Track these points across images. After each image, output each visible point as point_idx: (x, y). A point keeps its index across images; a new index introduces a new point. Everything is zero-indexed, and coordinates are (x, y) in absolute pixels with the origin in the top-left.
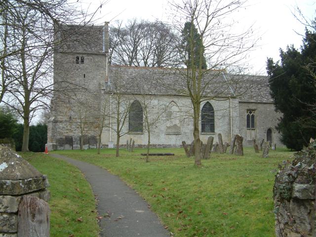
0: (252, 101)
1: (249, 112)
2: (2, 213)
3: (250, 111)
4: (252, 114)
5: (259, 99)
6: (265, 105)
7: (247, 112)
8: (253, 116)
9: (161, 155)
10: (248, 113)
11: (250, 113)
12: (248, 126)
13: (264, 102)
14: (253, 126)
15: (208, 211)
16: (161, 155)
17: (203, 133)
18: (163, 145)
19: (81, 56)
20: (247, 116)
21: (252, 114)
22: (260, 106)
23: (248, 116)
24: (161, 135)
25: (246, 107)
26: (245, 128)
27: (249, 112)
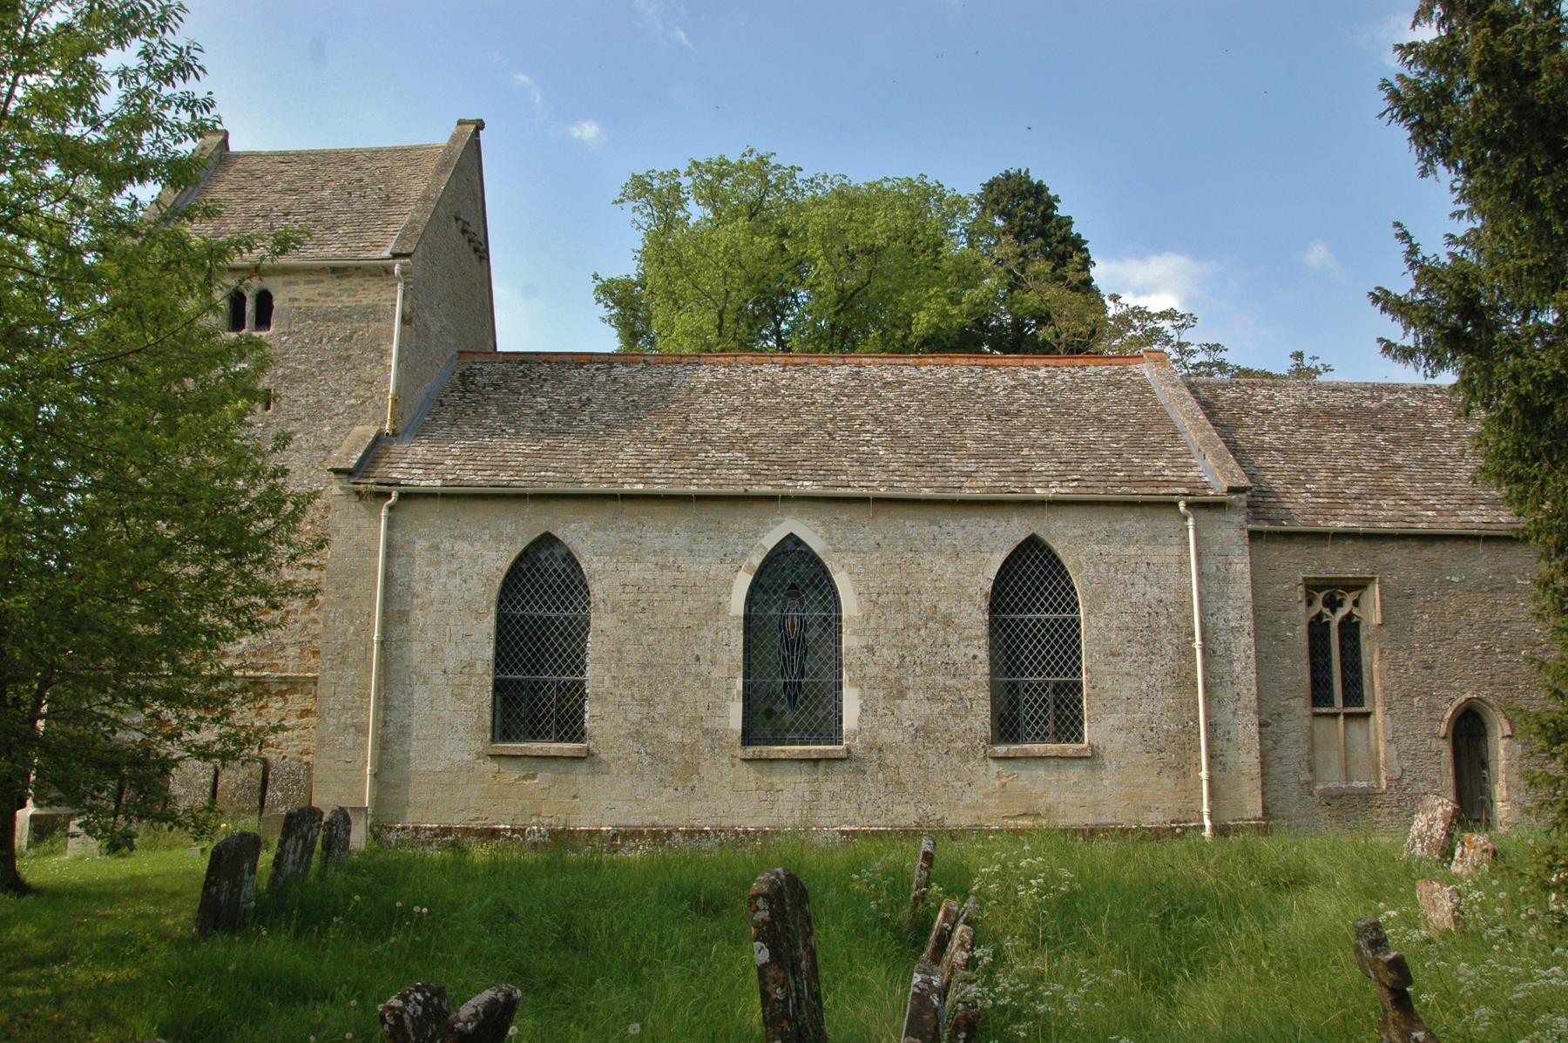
0: (1340, 525)
1: (1321, 596)
2: (543, 1040)
3: (1330, 591)
4: (1342, 613)
5: (1386, 516)
6: (1430, 553)
7: (1310, 603)
8: (1350, 628)
9: (339, 272)
10: (1318, 606)
11: (1333, 604)
12: (1320, 693)
13: (1422, 527)
14: (1354, 692)
15: (172, 224)
16: (339, 272)
17: (1001, 749)
18: (718, 831)
19: (255, 284)
20: (1311, 624)
21: (1342, 613)
22: (1392, 555)
23: (1318, 630)
24: (705, 766)
25: (1299, 565)
26: (1300, 705)
27: (1321, 596)
